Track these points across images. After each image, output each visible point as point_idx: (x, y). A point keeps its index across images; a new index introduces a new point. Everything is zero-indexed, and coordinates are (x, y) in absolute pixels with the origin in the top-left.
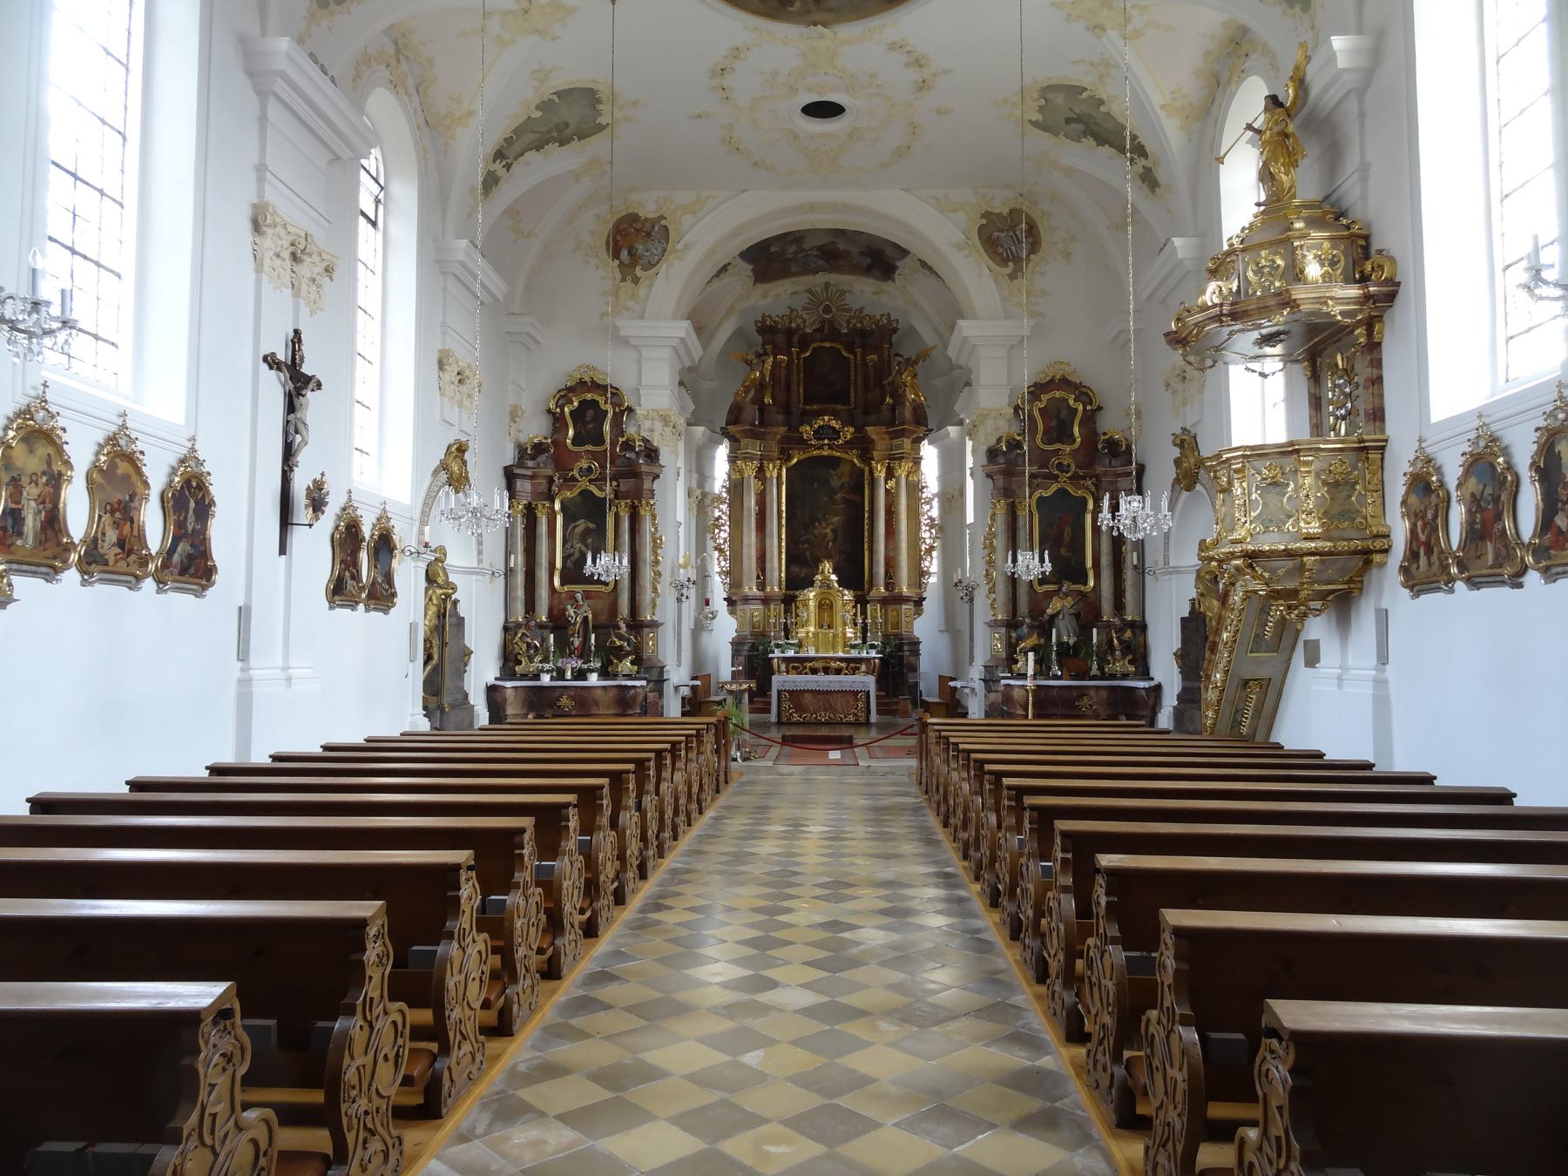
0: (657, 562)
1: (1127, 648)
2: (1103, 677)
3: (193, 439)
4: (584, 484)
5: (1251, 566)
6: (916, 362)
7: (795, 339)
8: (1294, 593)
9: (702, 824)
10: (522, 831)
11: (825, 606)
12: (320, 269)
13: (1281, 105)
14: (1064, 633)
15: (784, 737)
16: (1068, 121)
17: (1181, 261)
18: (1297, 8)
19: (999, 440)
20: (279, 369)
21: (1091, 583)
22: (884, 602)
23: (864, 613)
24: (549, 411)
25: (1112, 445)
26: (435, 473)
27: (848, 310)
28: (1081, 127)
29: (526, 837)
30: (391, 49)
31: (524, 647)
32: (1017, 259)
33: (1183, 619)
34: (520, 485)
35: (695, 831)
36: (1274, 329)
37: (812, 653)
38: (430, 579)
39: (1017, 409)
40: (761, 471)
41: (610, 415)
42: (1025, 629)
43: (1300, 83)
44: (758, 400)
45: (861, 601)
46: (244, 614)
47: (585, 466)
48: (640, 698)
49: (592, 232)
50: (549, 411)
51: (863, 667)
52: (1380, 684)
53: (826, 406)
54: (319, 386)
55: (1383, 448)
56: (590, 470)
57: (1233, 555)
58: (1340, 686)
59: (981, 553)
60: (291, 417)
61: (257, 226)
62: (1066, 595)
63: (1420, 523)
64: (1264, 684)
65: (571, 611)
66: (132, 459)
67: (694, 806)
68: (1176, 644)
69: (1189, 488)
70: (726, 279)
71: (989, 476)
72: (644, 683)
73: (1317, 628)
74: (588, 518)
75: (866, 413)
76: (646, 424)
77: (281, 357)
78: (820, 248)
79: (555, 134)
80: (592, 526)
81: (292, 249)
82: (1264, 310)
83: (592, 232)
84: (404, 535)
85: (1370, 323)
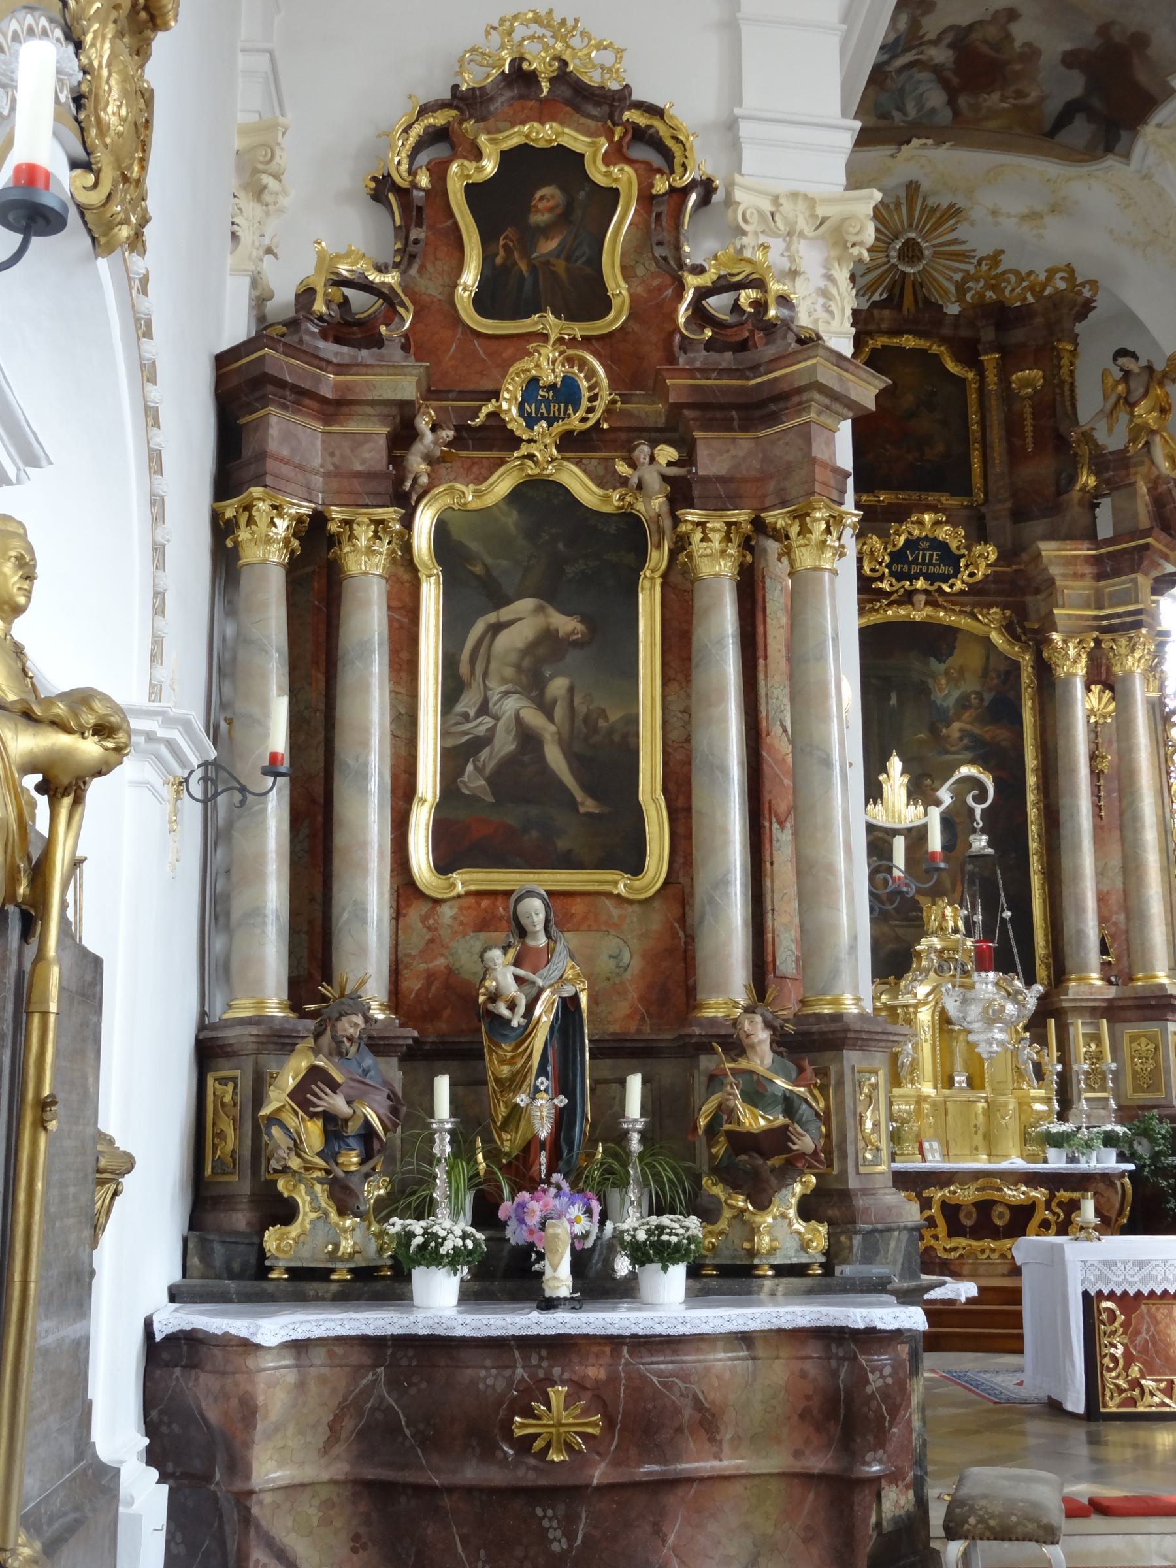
22: (1111, 1011)
27: (963, 256)
31: (313, 1133)
34: (284, 432)
37: (934, 1161)
41: (623, 220)
51: (1088, 1210)
65: (503, 974)
74: (550, 593)
80: (566, 624)
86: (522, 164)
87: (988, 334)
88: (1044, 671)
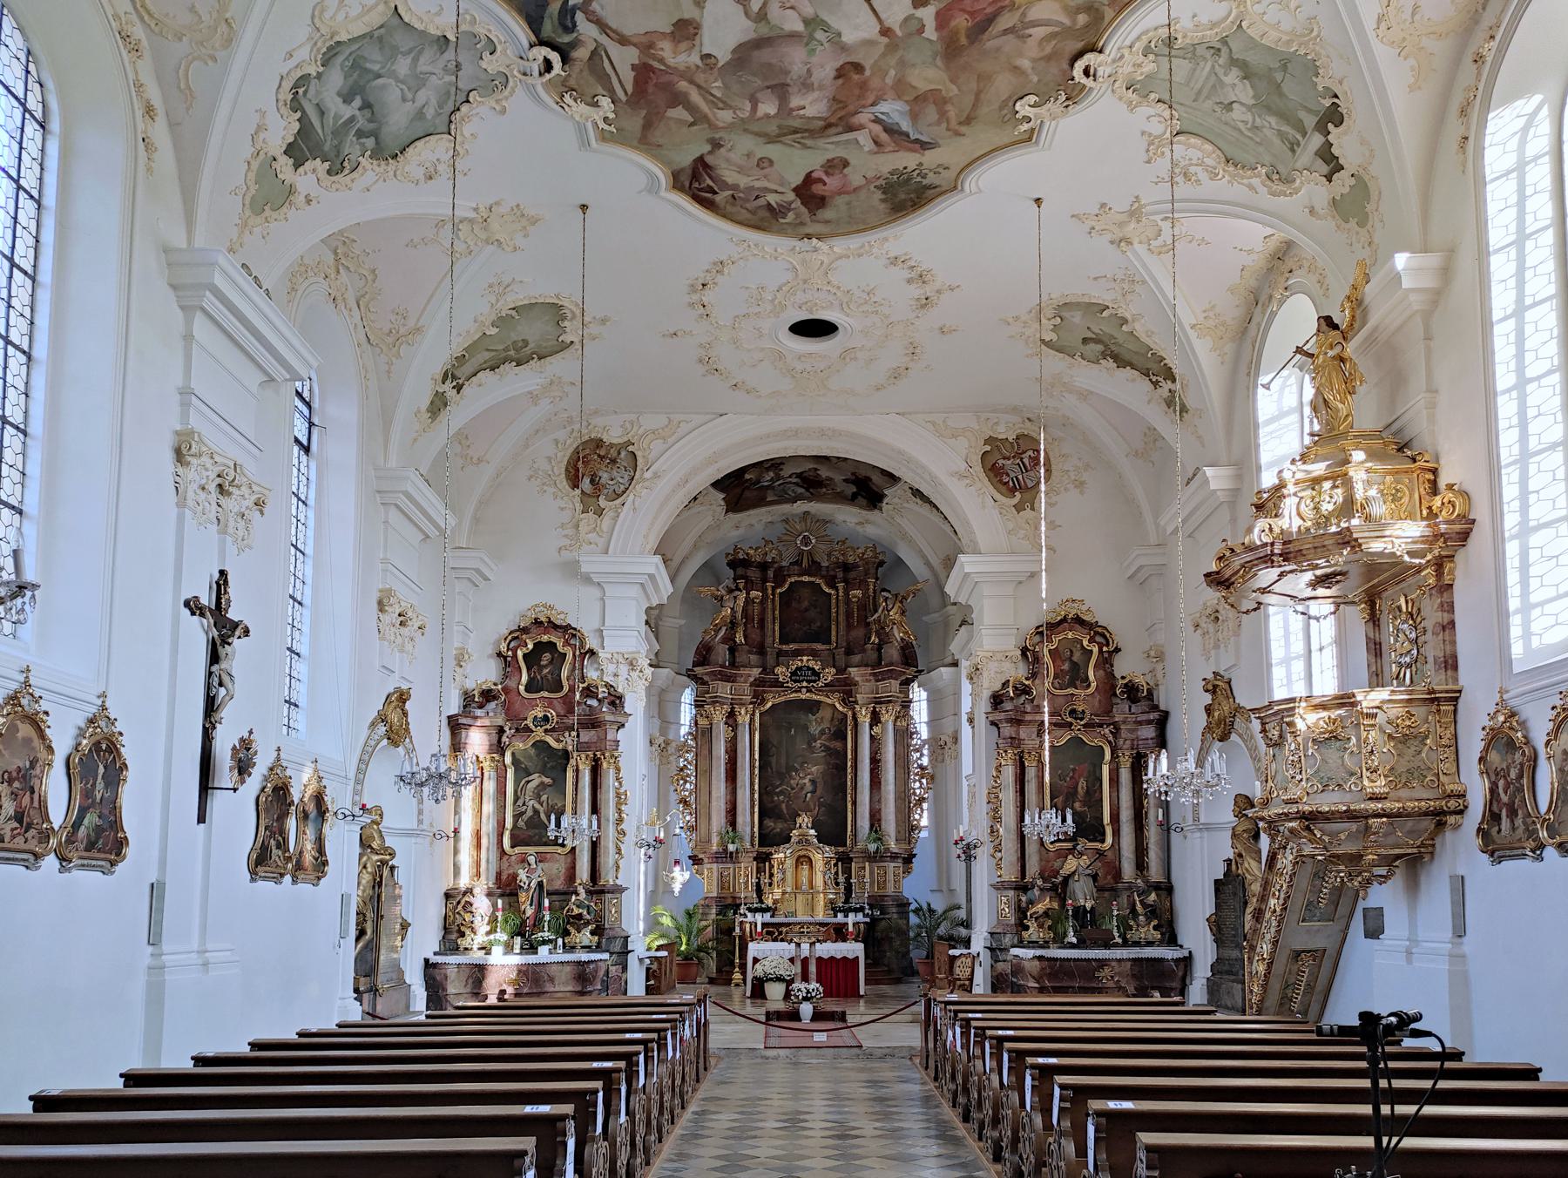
0: (620, 820)
1: (1152, 912)
2: (1126, 943)
3: (103, 695)
4: (539, 733)
5: (1308, 828)
6: (904, 598)
7: (771, 574)
8: (1357, 858)
9: (685, 1119)
10: (524, 1153)
11: (803, 860)
12: (250, 502)
13: (1336, 327)
14: (1083, 895)
15: (768, 1014)
16: (1085, 341)
17: (1215, 491)
18: (1353, 223)
19: (1005, 684)
20: (202, 615)
21: (1109, 840)
23: (847, 872)
24: (499, 654)
25: (1132, 691)
26: (373, 725)
27: (831, 541)
28: (1100, 347)
29: (527, 1159)
30: (330, 258)
32: (1023, 488)
33: (1216, 882)
35: (678, 1131)
36: (1329, 570)
38: (365, 844)
39: (1024, 651)
40: (731, 715)
42: (1036, 892)
43: (1357, 303)
44: (729, 639)
45: (844, 860)
46: (156, 891)
47: (540, 715)
48: (601, 973)
49: (549, 459)
50: (499, 654)
52: (1457, 958)
53: (805, 646)
54: (247, 632)
55: (1456, 699)
56: (546, 719)
57: (1287, 817)
58: (1409, 961)
59: (983, 808)
60: (215, 668)
61: (179, 456)
62: (1081, 854)
63: (1501, 783)
64: (1317, 955)
66: (36, 722)
67: (677, 1101)
68: (1210, 909)
69: (1224, 738)
70: (696, 508)
71: (993, 723)
72: (606, 956)
73: (1385, 896)
74: (543, 772)
75: (849, 652)
76: (610, 668)
77: (204, 601)
78: (799, 475)
79: (512, 353)
81: (219, 480)
82: (1321, 549)
83: (549, 459)
84: (338, 798)
85: (1439, 564)
86: (540, 647)
87: (840, 575)
88: (855, 718)
